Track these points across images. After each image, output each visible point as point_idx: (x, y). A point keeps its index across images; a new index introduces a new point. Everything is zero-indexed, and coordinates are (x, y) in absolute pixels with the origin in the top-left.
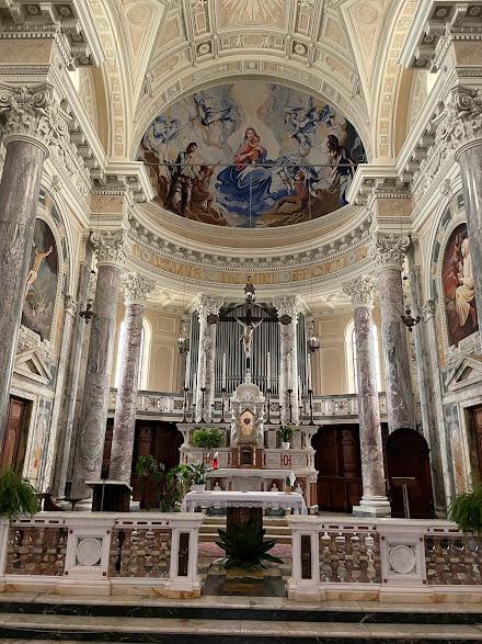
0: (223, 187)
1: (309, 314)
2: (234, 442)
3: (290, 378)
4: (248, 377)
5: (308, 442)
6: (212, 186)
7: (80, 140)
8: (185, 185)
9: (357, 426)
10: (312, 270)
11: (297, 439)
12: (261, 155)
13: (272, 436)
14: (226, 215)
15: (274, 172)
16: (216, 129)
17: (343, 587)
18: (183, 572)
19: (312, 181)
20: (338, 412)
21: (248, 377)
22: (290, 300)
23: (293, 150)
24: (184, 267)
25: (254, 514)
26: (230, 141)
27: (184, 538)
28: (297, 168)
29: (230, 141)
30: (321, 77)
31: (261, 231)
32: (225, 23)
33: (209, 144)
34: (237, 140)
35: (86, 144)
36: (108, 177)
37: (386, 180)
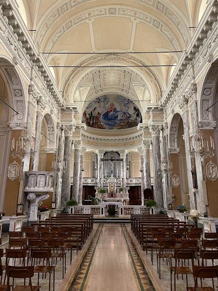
0: (104, 118)
1: (130, 153)
2: (109, 192)
3: (124, 173)
4: (112, 176)
5: (127, 191)
6: (101, 119)
7: (27, 47)
8: (93, 119)
9: (140, 186)
10: (130, 143)
11: (124, 191)
12: (115, 109)
13: (118, 190)
14: (105, 126)
15: (119, 113)
16: (102, 104)
17: (128, 216)
18: (102, 214)
19: (129, 117)
20: (137, 182)
21: (112, 176)
22: (123, 152)
23: (124, 109)
24: (93, 143)
25: (114, 206)
26: (106, 106)
27: (102, 209)
28: (125, 113)
29: (106, 106)
30: (130, 96)
31: (115, 131)
32: (105, 86)
33: (100, 107)
34: (108, 106)
35: (27, 42)
36: (67, 108)
37: (155, 108)
